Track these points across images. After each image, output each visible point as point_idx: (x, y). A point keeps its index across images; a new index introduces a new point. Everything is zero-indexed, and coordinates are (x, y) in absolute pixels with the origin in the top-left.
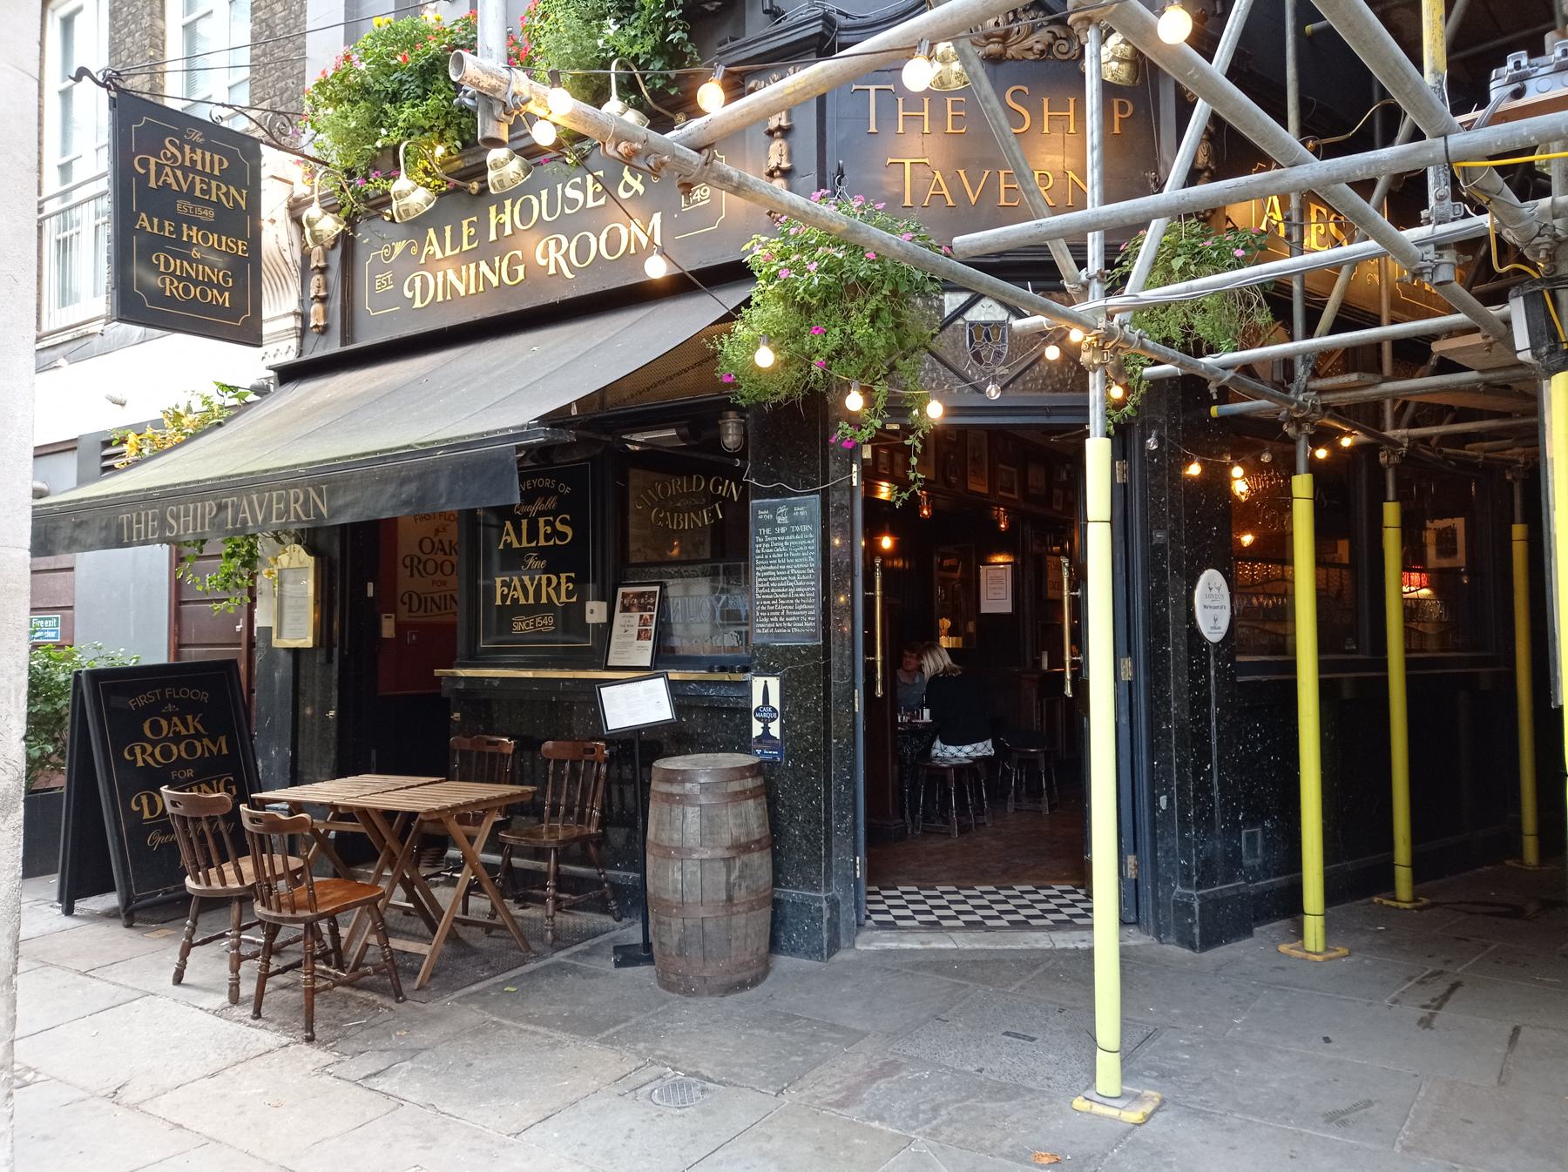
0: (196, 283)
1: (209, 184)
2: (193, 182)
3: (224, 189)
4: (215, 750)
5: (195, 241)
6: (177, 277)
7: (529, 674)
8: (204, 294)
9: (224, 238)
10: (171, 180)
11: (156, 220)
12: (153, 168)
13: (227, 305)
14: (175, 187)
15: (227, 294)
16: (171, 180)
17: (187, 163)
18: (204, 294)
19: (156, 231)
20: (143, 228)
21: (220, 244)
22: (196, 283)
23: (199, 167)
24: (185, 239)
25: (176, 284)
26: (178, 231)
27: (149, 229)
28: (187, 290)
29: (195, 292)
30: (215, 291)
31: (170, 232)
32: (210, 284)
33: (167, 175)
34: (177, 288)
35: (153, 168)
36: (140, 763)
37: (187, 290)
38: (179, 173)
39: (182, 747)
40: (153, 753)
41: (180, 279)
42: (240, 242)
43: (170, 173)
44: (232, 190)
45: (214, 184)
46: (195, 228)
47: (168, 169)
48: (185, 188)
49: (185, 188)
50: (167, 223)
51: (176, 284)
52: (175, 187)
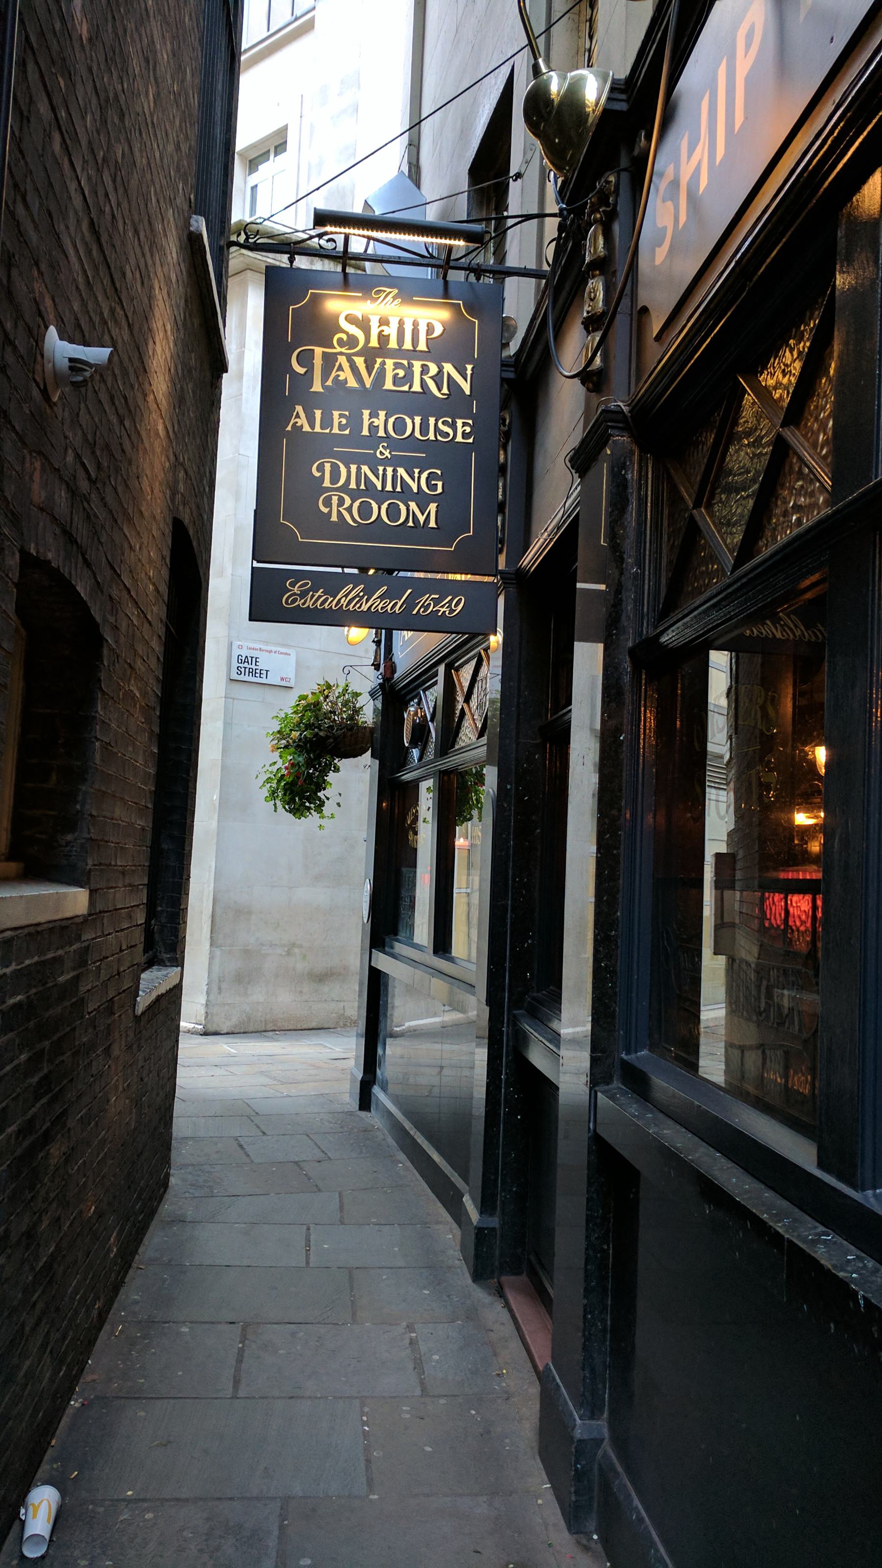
0: (381, 496)
1: (409, 370)
2: (382, 371)
3: (433, 369)
4: (422, 519)
5: (381, 433)
6: (351, 493)
7: (865, 133)
8: (393, 512)
9: (432, 421)
10: (346, 374)
11: (318, 413)
12: (318, 362)
13: (432, 524)
14: (352, 383)
15: (433, 507)
16: (346, 374)
17: (374, 343)
18: (393, 512)
19: (318, 429)
20: (297, 429)
21: (424, 429)
22: (381, 496)
23: (393, 344)
24: (365, 432)
25: (348, 502)
26: (355, 422)
27: (306, 428)
28: (365, 511)
29: (379, 511)
30: (413, 505)
31: (341, 427)
32: (406, 494)
33: (340, 368)
34: (349, 510)
35: (318, 362)
36: (334, 518)
37: (365, 511)
38: (360, 361)
39: (384, 507)
40: (351, 506)
41: (354, 495)
42: (459, 422)
43: (346, 365)
44: (448, 368)
45: (417, 366)
46: (382, 414)
47: (342, 360)
48: (368, 382)
49: (368, 382)
50: (336, 414)
51: (348, 502)
52: (352, 383)
